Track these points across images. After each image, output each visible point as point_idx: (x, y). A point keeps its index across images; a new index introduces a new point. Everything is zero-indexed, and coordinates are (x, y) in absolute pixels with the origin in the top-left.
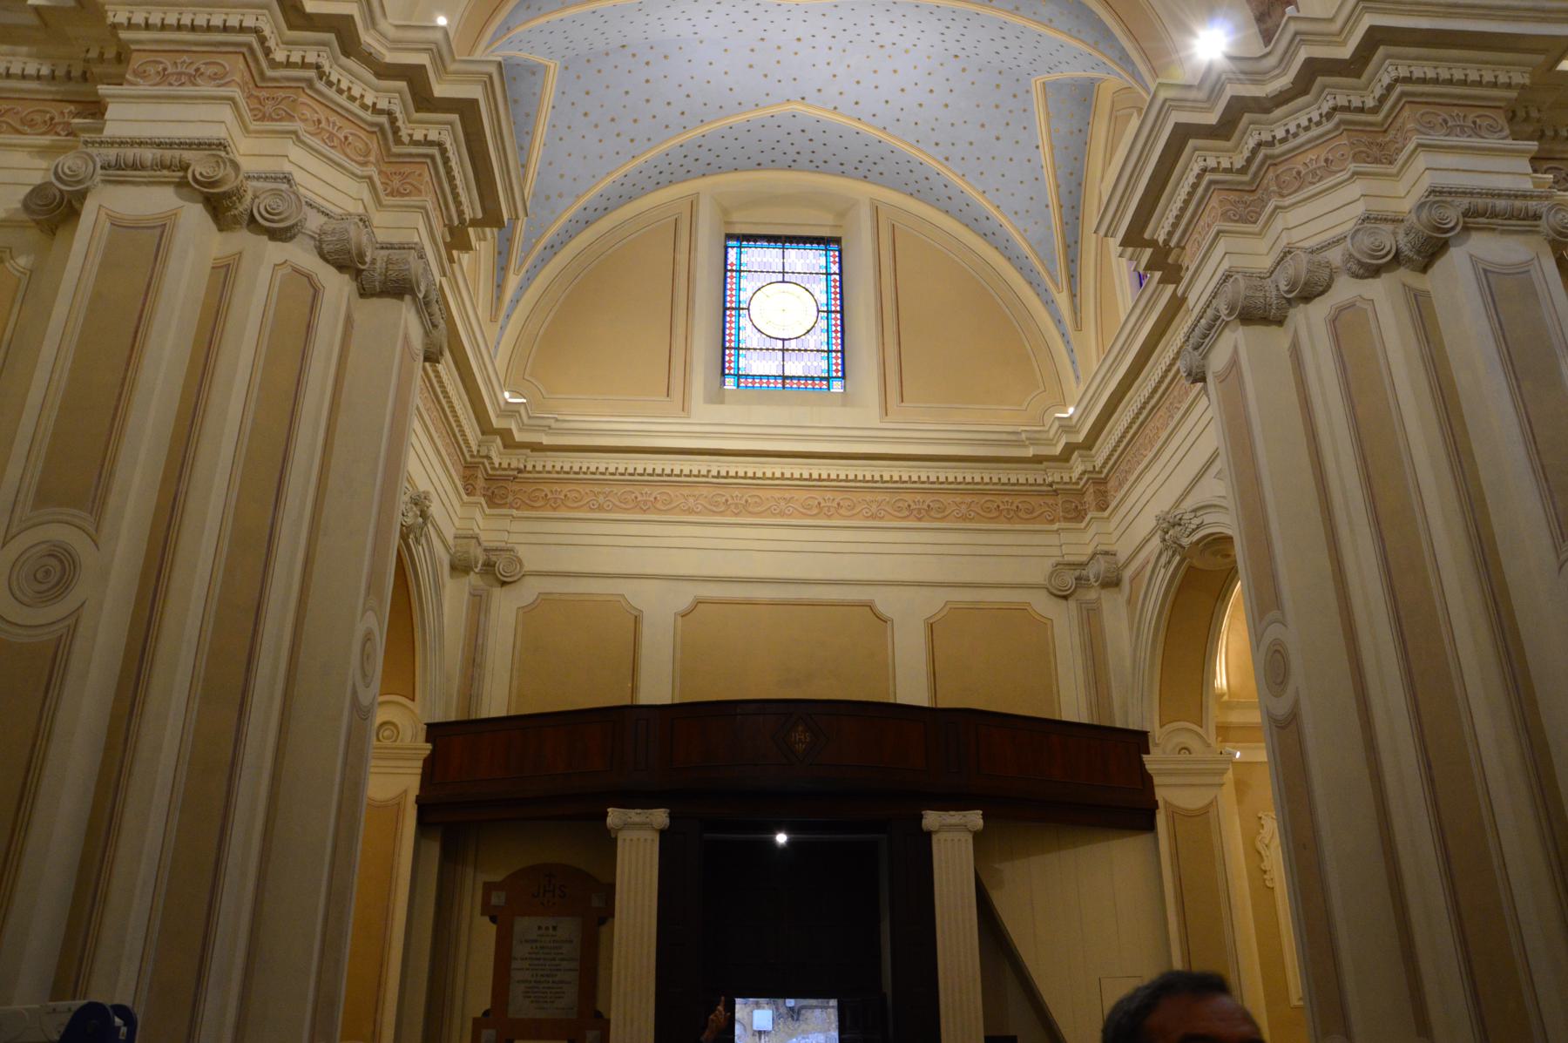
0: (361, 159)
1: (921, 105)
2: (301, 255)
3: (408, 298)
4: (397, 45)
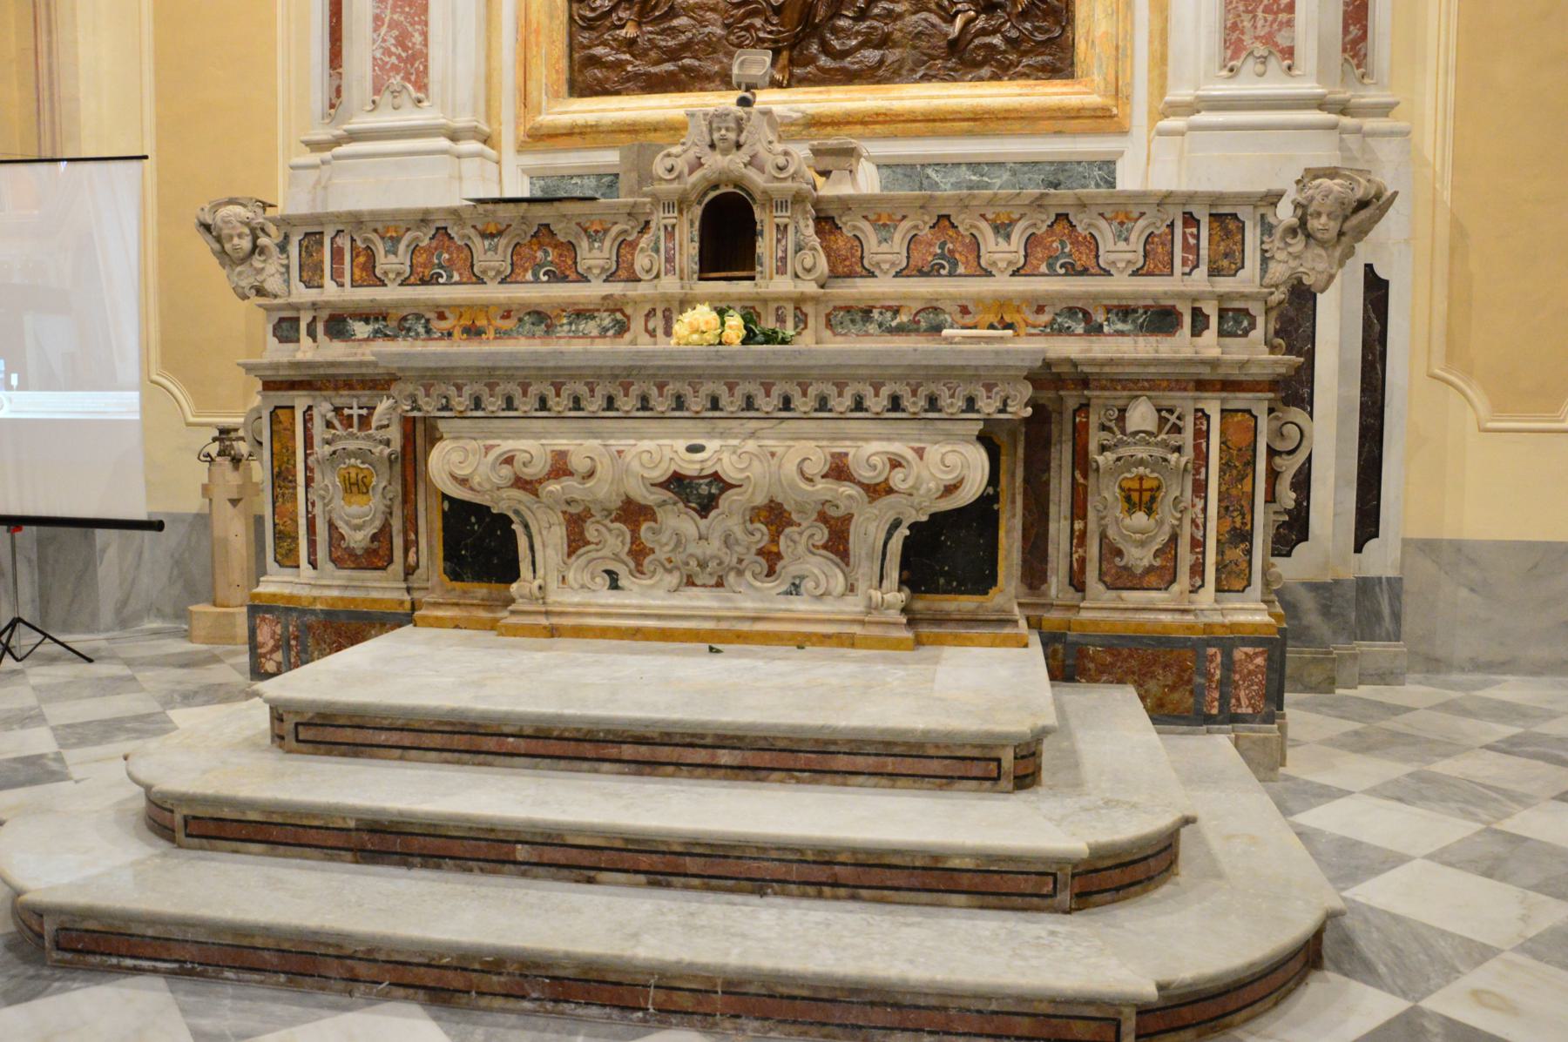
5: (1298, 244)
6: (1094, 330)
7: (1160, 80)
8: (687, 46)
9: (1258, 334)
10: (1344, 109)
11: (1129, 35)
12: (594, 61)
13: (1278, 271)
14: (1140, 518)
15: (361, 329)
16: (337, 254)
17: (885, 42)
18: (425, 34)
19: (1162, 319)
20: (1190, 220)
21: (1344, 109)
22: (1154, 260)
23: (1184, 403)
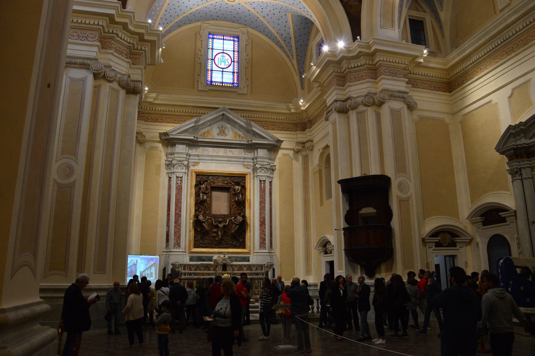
0: (126, 56)
1: (268, 15)
2: (115, 85)
3: (138, 95)
4: (136, 26)
5: (267, 268)
6: (253, 275)
7: (254, 250)
8: (207, 244)
9: (264, 275)
10: (270, 253)
11: (251, 245)
12: (196, 244)
13: (266, 270)
14: (257, 290)
15: (193, 275)
16: (187, 268)
17: (227, 244)
18: (180, 241)
19: (257, 274)
20: (259, 266)
21: (270, 253)
22: (256, 269)
23: (259, 281)
